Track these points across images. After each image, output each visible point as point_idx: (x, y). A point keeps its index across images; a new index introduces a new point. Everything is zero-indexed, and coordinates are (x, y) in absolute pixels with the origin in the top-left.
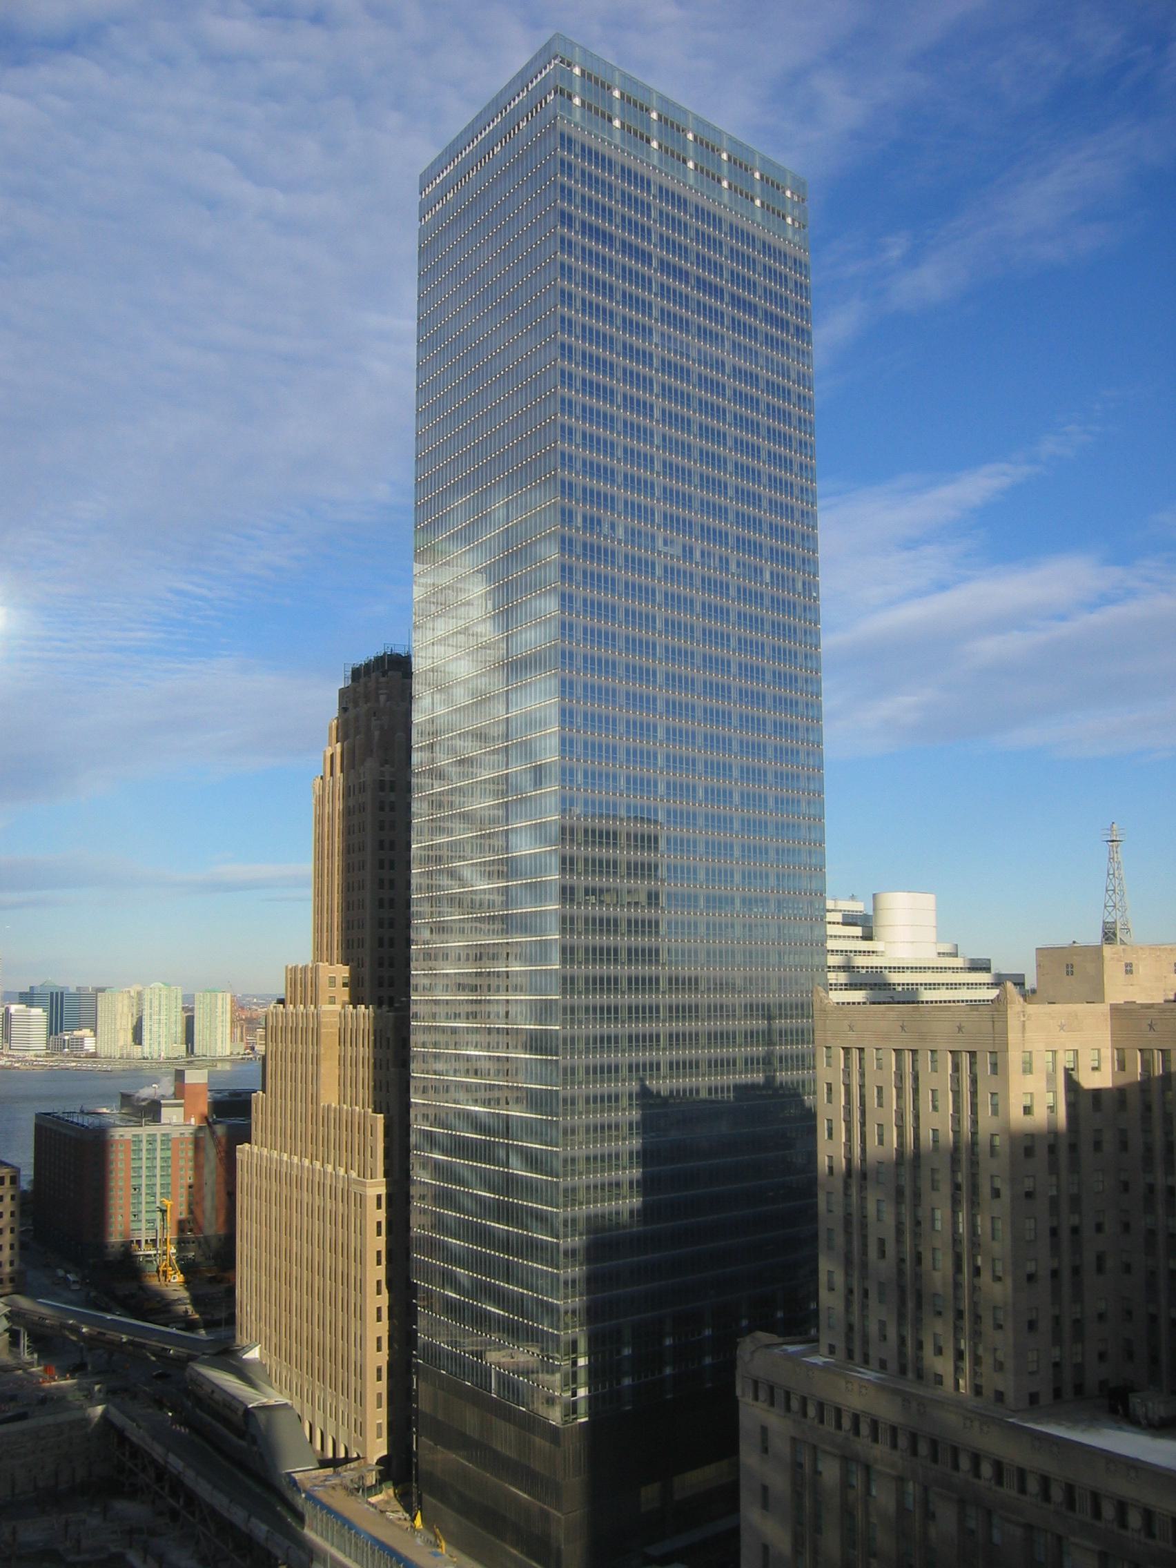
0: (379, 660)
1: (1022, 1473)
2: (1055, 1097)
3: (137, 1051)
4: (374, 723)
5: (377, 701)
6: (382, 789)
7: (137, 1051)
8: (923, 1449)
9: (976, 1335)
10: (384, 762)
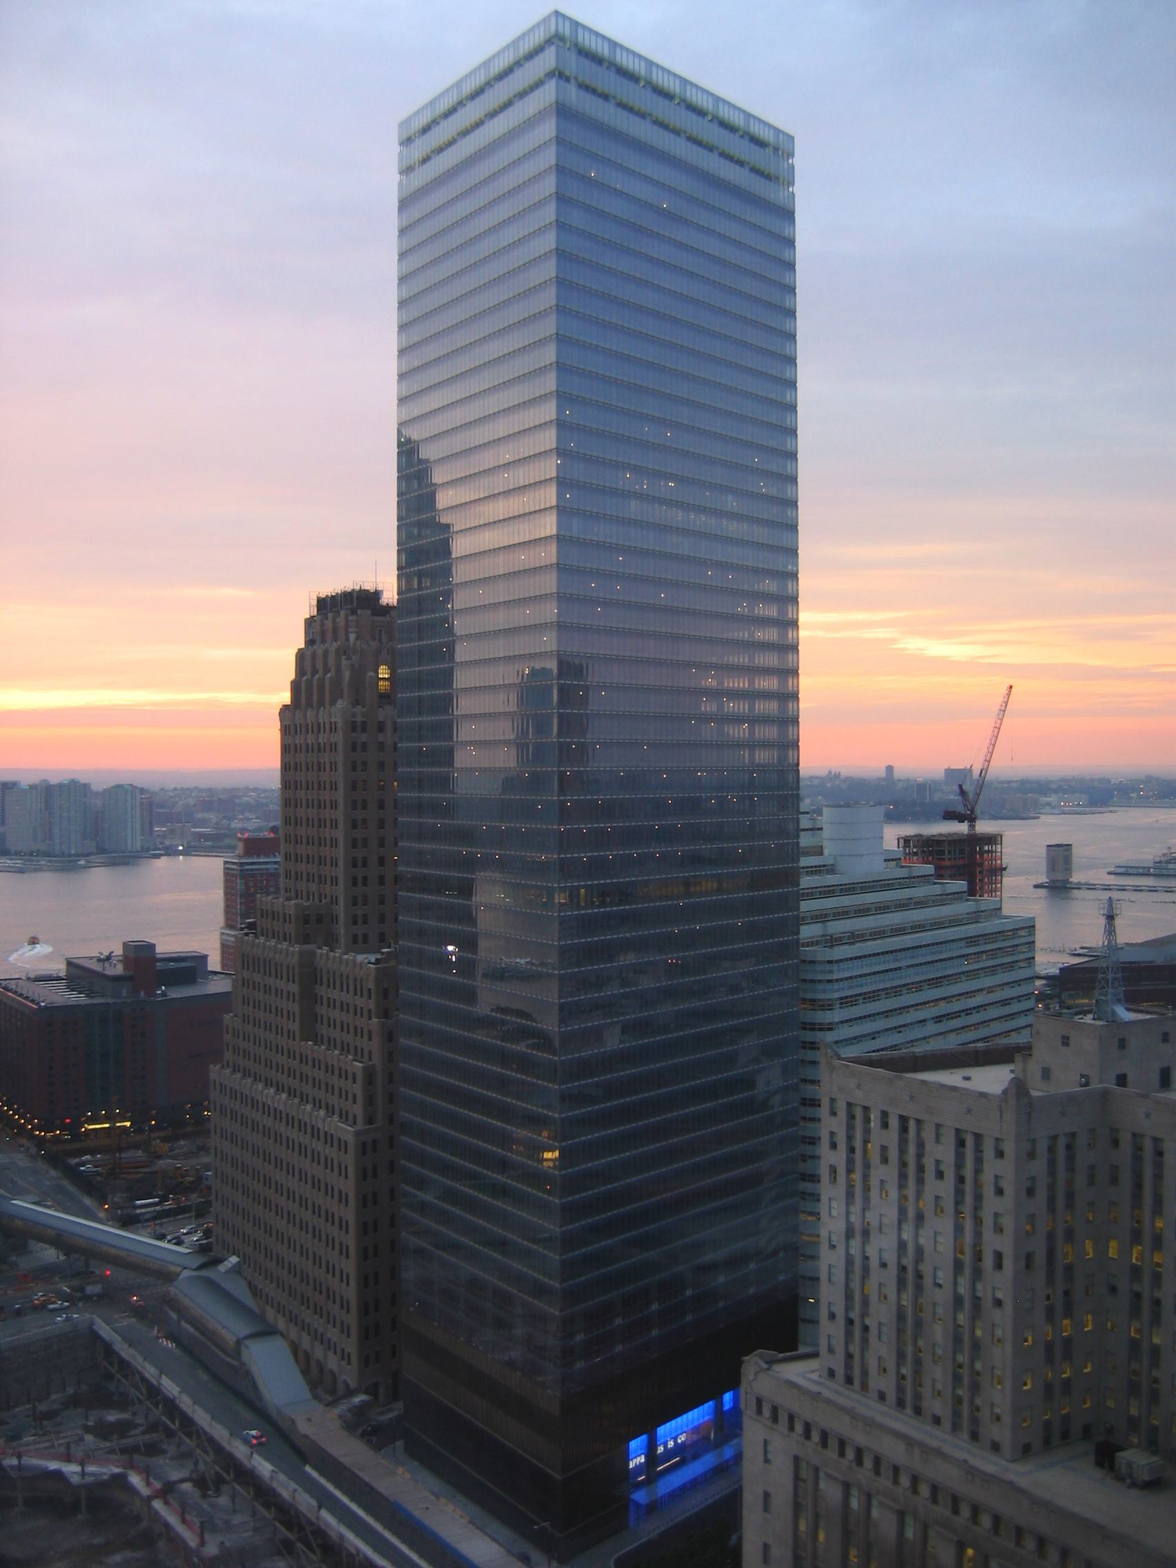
1: (896, 1470)
2: (1153, 1224)
5: (347, 639)
6: (354, 729)
10: (357, 702)
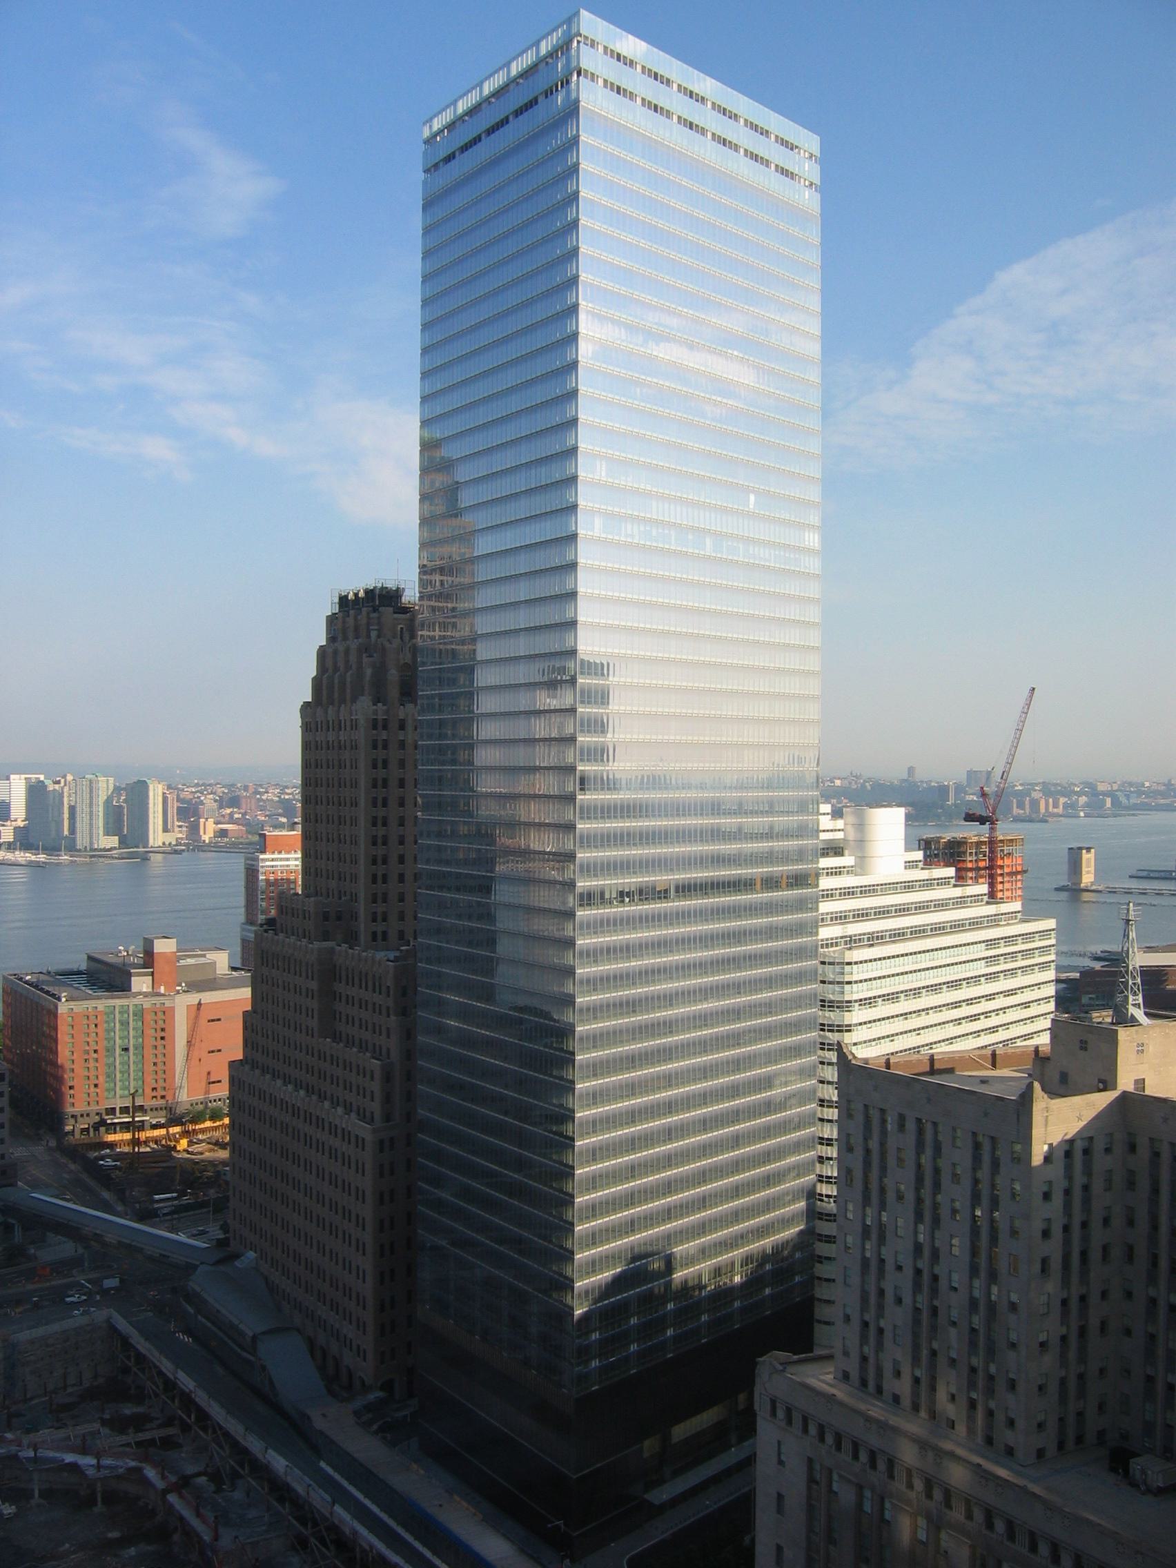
0: (369, 593)
3: (7, 1126)
4: (365, 660)
5: (369, 636)
7: (7, 1126)
8: (829, 1439)
9: (880, 1346)
10: (377, 700)
